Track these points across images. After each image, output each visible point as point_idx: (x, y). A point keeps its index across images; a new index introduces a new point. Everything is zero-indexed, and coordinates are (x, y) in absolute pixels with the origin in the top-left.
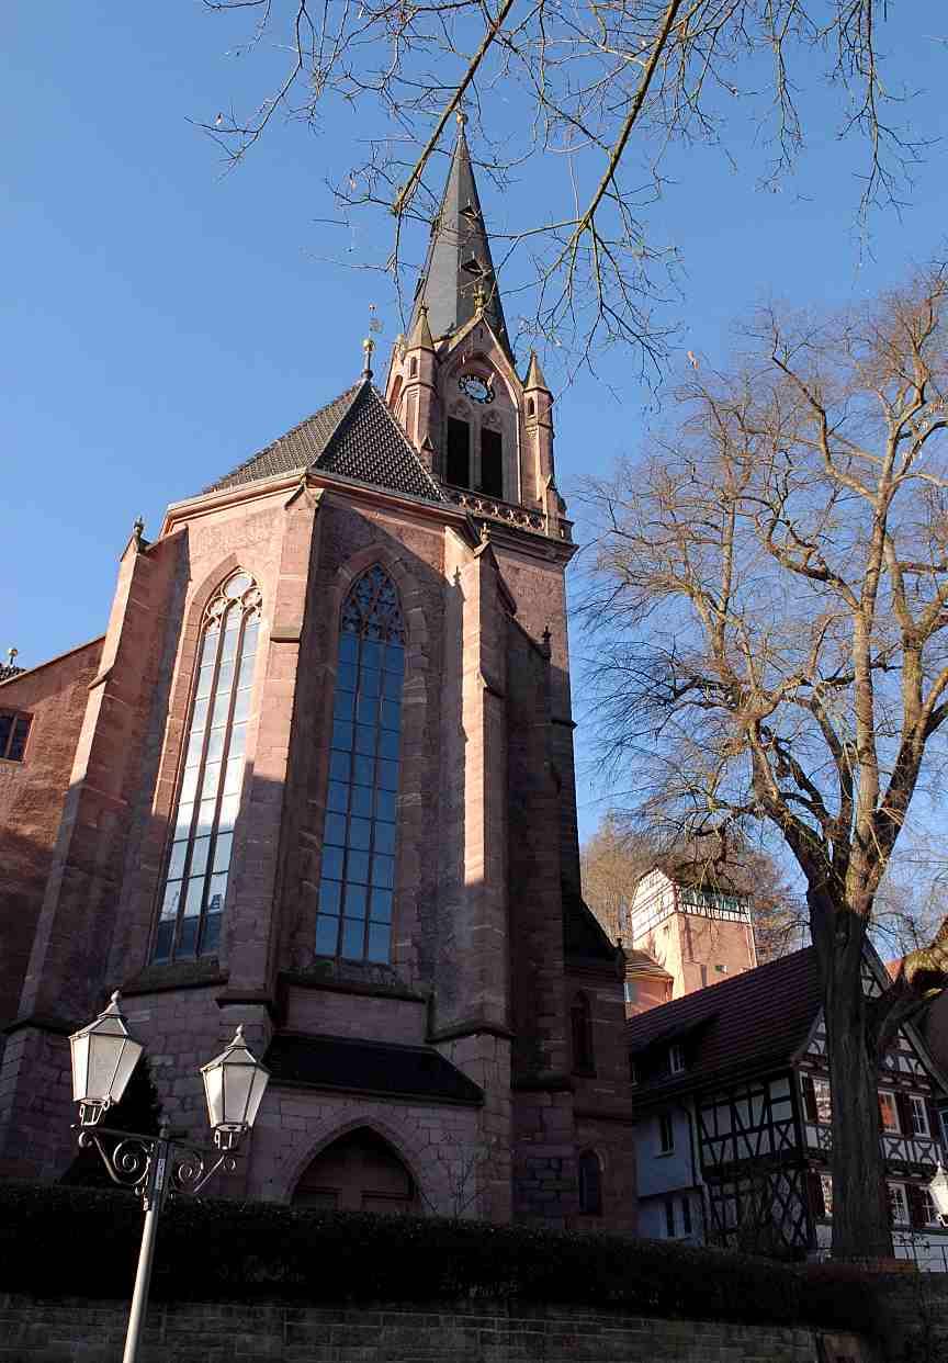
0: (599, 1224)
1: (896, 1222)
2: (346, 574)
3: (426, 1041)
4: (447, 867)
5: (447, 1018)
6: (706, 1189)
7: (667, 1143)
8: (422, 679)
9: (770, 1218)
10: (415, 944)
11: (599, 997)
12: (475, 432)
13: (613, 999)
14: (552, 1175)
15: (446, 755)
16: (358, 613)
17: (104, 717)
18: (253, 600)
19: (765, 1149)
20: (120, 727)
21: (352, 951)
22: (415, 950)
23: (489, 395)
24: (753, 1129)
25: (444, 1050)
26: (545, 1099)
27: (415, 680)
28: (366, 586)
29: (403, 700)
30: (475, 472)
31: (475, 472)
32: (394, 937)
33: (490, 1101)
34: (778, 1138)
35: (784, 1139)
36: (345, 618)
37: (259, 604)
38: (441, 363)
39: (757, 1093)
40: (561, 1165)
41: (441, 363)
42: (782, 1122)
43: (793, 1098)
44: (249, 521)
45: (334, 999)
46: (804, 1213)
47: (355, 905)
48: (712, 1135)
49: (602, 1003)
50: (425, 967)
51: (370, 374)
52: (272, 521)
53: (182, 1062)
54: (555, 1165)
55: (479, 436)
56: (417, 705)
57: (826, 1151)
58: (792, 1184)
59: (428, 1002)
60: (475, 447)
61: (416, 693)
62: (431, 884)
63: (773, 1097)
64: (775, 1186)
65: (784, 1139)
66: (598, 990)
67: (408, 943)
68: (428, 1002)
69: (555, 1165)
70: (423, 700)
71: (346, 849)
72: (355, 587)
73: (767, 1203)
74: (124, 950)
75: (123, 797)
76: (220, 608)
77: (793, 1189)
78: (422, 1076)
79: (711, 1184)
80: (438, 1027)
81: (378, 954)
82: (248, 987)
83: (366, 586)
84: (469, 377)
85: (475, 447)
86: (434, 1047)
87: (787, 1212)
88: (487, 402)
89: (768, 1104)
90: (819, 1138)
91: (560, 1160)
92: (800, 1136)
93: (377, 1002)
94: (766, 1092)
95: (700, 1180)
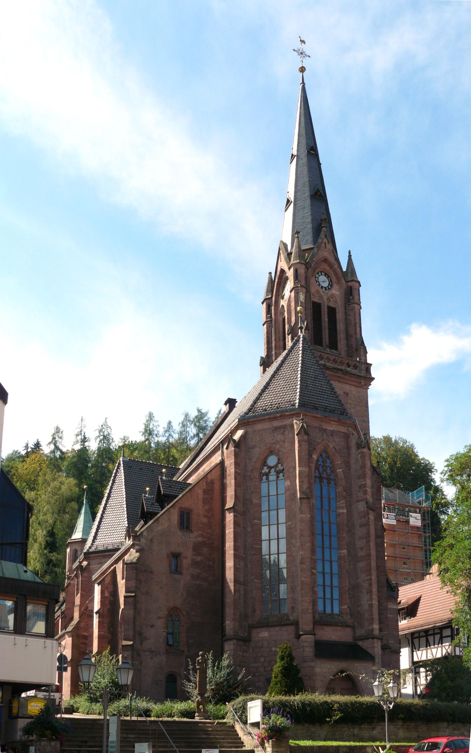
1: (384, 490)
2: (315, 457)
4: (357, 578)
5: (360, 632)
8: (344, 501)
10: (348, 607)
11: (389, 606)
12: (324, 311)
18: (280, 467)
20: (239, 526)
22: (348, 609)
25: (360, 643)
29: (338, 510)
37: (283, 470)
39: (437, 634)
44: (276, 429)
45: (327, 629)
49: (390, 609)
52: (284, 431)
55: (326, 310)
56: (343, 513)
57: (346, 502)
59: (353, 627)
60: (325, 318)
61: (342, 508)
63: (444, 635)
67: (346, 607)
70: (345, 511)
72: (318, 461)
74: (254, 611)
75: (244, 554)
76: (265, 470)
82: (308, 629)
84: (320, 274)
85: (325, 318)
86: (357, 642)
90: (460, 651)
93: (339, 628)
94: (441, 633)
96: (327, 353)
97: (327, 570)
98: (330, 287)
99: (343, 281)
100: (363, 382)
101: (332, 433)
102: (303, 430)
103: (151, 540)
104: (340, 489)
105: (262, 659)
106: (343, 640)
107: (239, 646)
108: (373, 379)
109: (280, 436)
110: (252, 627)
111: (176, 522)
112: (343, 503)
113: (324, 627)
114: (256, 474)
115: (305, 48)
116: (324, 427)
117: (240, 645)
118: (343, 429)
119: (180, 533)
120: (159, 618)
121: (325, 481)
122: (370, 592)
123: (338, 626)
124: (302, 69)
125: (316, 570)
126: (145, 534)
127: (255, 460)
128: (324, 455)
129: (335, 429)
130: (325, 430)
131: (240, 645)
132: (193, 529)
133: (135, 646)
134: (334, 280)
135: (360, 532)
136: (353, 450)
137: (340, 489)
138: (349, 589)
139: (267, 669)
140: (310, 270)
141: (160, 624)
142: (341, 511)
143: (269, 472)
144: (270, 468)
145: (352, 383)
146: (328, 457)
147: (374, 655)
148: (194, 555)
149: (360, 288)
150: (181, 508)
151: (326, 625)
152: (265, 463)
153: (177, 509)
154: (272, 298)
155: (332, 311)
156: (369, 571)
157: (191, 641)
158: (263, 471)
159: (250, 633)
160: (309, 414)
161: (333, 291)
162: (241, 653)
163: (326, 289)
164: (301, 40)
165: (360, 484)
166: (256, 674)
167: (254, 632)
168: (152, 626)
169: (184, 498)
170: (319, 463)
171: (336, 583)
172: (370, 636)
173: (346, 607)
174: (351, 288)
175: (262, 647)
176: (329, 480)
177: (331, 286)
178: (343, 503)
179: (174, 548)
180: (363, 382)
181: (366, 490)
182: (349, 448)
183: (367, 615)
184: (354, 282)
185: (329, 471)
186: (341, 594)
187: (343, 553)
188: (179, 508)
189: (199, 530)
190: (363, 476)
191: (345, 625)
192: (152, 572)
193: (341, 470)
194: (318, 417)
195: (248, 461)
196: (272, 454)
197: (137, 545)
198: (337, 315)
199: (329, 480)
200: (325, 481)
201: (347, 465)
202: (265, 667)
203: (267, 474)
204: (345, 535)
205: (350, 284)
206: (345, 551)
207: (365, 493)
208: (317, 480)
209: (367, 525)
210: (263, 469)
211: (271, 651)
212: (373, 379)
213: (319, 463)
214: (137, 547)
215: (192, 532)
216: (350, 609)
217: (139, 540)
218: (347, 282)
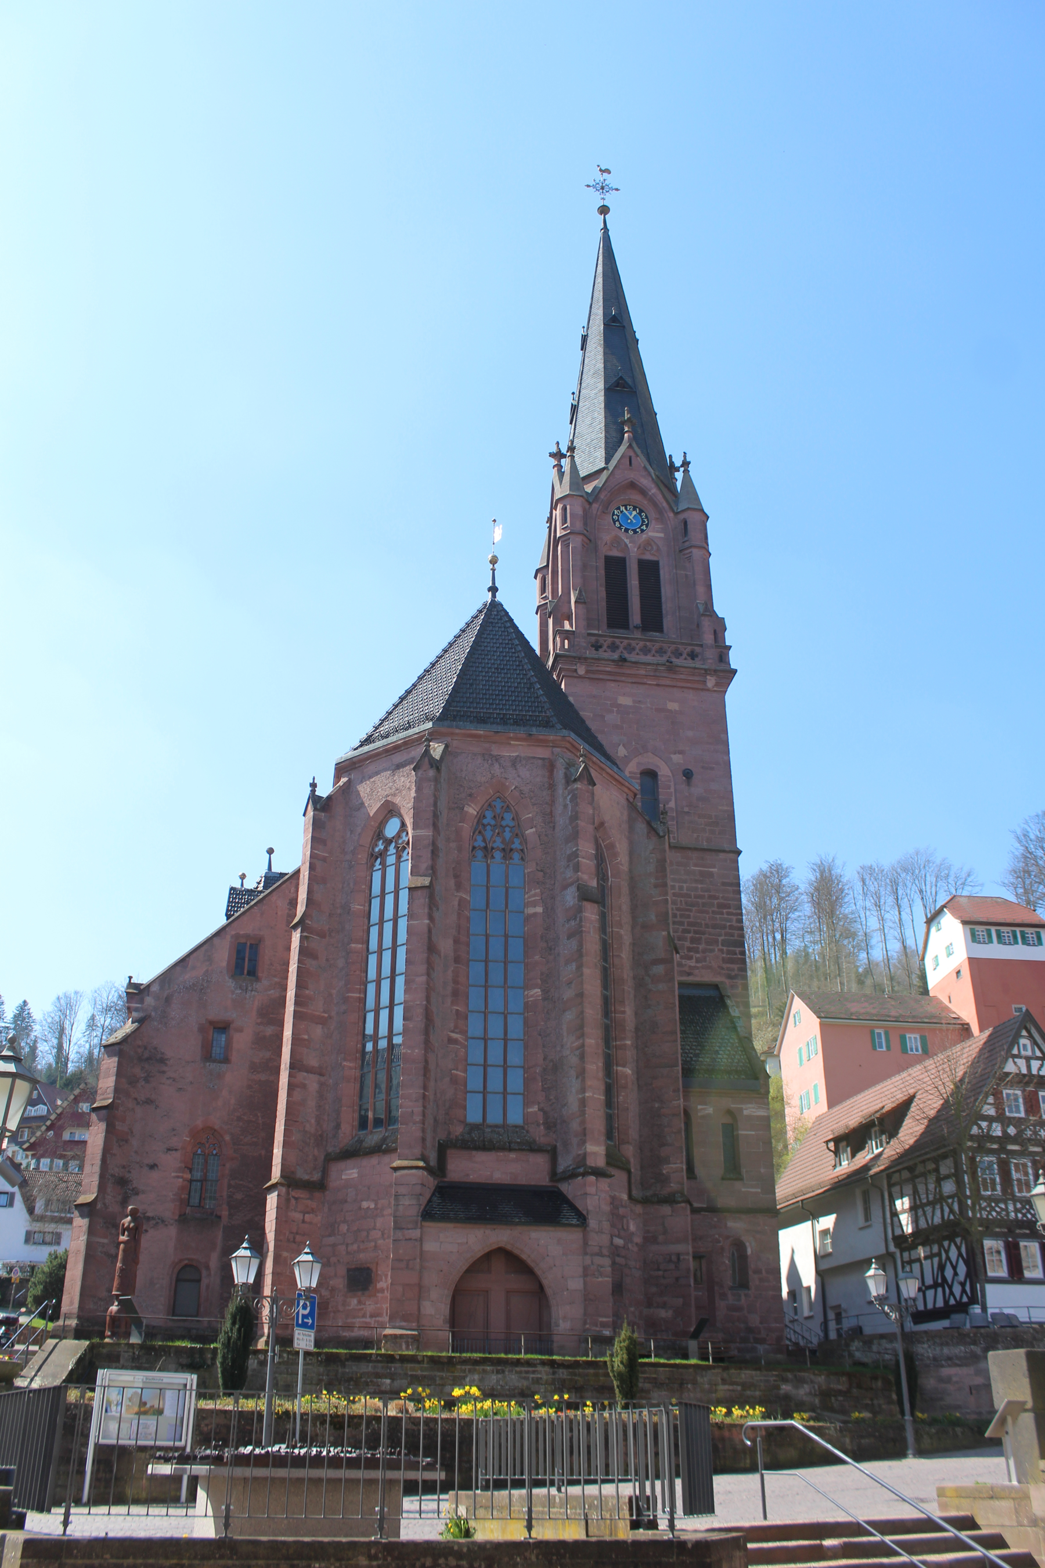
0: (746, 1295)
3: (551, 1180)
5: (564, 1163)
6: (898, 1255)
7: (867, 1217)
9: (944, 1278)
10: (541, 1109)
11: (745, 1112)
13: (762, 1113)
14: (672, 1266)
15: (559, 954)
16: (484, 840)
17: (302, 951)
19: (937, 1220)
21: (494, 1117)
23: (643, 521)
24: (929, 1203)
25: (565, 1188)
26: (666, 1209)
27: (533, 892)
28: (489, 814)
30: (635, 616)
31: (635, 616)
32: (526, 1104)
33: (592, 1223)
34: (947, 1210)
35: (952, 1211)
36: (474, 848)
38: (590, 504)
40: (679, 1259)
41: (590, 504)
42: (949, 1197)
43: (957, 1176)
45: (480, 1156)
46: (968, 1275)
47: (495, 1082)
48: (924, 1201)
49: (749, 1118)
50: (550, 1125)
51: (493, 589)
53: (379, 1206)
54: (674, 1258)
56: (535, 914)
58: (959, 1248)
61: (534, 904)
62: (552, 1061)
64: (947, 1252)
65: (952, 1211)
66: (744, 1106)
67: (535, 1108)
68: (553, 1153)
69: (674, 1258)
70: (539, 910)
71: (485, 1040)
72: (481, 817)
73: (942, 1268)
74: (338, 1126)
75: (324, 1012)
76: (381, 846)
77: (960, 1255)
78: (547, 1205)
79: (902, 1251)
80: (560, 1168)
81: (515, 1117)
83: (489, 814)
87: (956, 1274)
88: (642, 531)
89: (939, 1181)
91: (678, 1255)
92: (1016, 1215)
95: (892, 1248)
96: (674, 643)
97: (496, 1028)
98: (644, 527)
99: (671, 515)
100: (711, 681)
101: (515, 762)
102: (426, 759)
103: (168, 1000)
104: (531, 868)
105: (344, 1228)
106: (522, 1180)
107: (293, 1201)
108: (735, 672)
109: (403, 779)
110: (331, 1159)
111: (224, 964)
112: (535, 895)
113: (474, 1153)
114: (363, 857)
115: (611, 180)
116: (494, 753)
117: (296, 1199)
118: (542, 752)
119: (230, 983)
120: (169, 1150)
121: (498, 855)
122: (582, 1074)
123: (510, 1150)
124: (604, 210)
125: (464, 1032)
126: (155, 988)
127: (359, 830)
128: (498, 804)
129: (522, 755)
130: (497, 759)
131: (296, 1199)
132: (260, 975)
133: (99, 1206)
134: (652, 514)
135: (567, 947)
136: (560, 790)
137: (531, 868)
138: (545, 1070)
139: (350, 1248)
140: (595, 506)
141: (171, 1162)
142: (531, 910)
143: (386, 849)
144: (388, 842)
145: (689, 685)
146: (508, 809)
147: (585, 1213)
148: (258, 1024)
149: (708, 524)
150: (237, 936)
151: (477, 1148)
152: (379, 834)
153: (228, 937)
154: (548, 565)
155: (649, 570)
156: (579, 1030)
157: (239, 1196)
158: (377, 850)
159: (325, 1172)
160: (457, 731)
161: (650, 534)
162: (298, 1216)
163: (635, 532)
164: (601, 170)
165: (568, 852)
166: (333, 1260)
167: (335, 1168)
168: (153, 1167)
169: (245, 918)
170: (485, 821)
171: (515, 1057)
172: (582, 1170)
173: (535, 1108)
174: (685, 523)
175: (346, 1201)
176: (507, 852)
177: (647, 526)
178: (535, 895)
179: (215, 1013)
180: (711, 681)
181: (578, 862)
182: (552, 787)
183: (575, 1125)
184: (689, 512)
185: (507, 835)
186: (527, 1082)
187: (532, 996)
188: (232, 937)
189: (275, 976)
190: (574, 836)
191: (532, 1148)
192: (162, 1061)
193: (534, 830)
194: (479, 736)
195: (349, 833)
196: (392, 816)
197: (136, 1010)
198: (662, 572)
199: (507, 852)
200: (516, 856)
201: (549, 818)
202: (347, 1245)
203: (383, 854)
204: (537, 957)
205: (682, 516)
206: (537, 991)
207: (577, 868)
208: (480, 854)
209: (577, 933)
210: (377, 845)
211: (360, 1208)
212: (735, 672)
213: (485, 821)
214: (135, 1014)
215: (258, 979)
216: (545, 1113)
217: (142, 1001)
218: (677, 514)
